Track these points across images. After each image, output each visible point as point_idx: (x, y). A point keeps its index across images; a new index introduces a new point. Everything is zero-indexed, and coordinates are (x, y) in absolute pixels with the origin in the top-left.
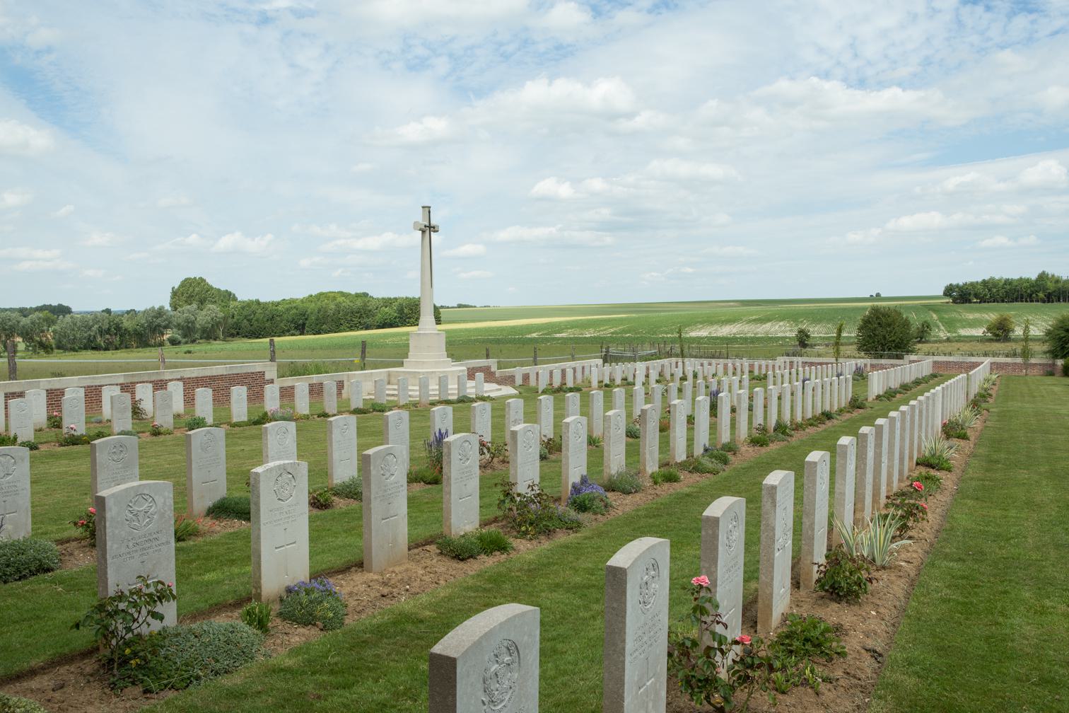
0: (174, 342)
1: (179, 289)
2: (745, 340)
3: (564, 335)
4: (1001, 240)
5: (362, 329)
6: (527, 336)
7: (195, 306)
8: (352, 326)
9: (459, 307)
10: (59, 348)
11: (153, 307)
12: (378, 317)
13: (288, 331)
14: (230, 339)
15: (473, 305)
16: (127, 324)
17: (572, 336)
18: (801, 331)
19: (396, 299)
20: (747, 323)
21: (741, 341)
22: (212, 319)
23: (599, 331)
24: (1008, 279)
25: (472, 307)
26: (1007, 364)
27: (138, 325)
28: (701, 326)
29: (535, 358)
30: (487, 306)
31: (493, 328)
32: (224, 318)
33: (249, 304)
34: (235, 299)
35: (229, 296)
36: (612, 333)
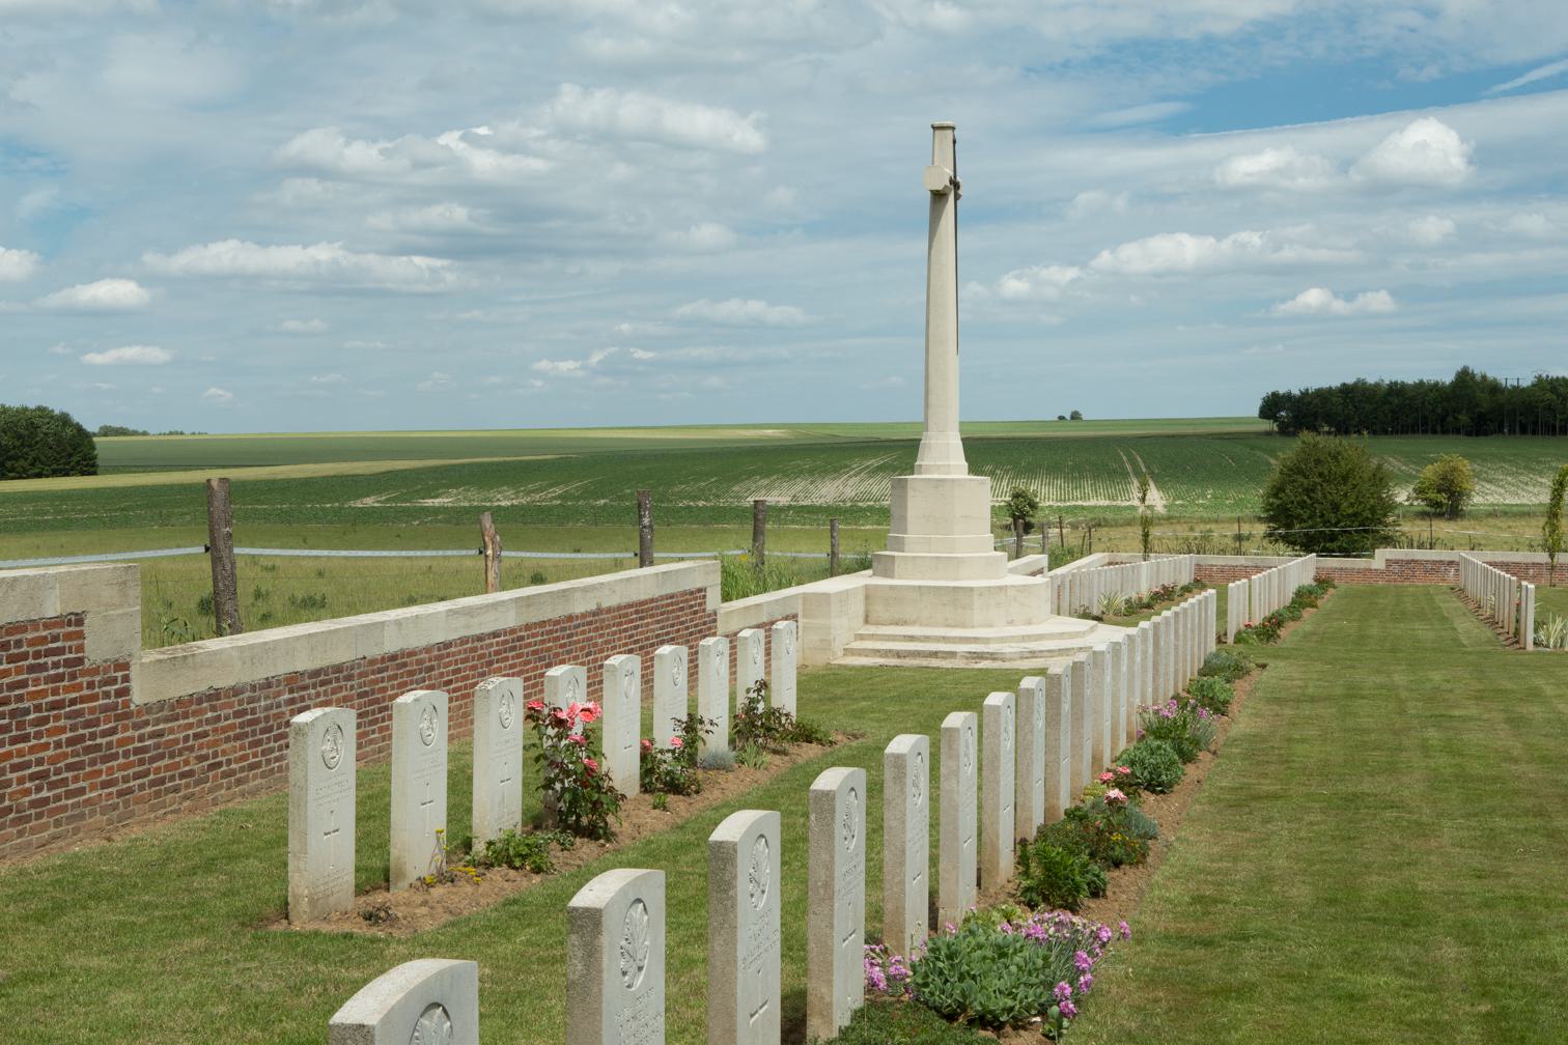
4: (1313, 297)
6: (352, 504)
9: (105, 435)
15: (141, 430)
24: (1396, 383)
25: (135, 433)
30: (177, 433)
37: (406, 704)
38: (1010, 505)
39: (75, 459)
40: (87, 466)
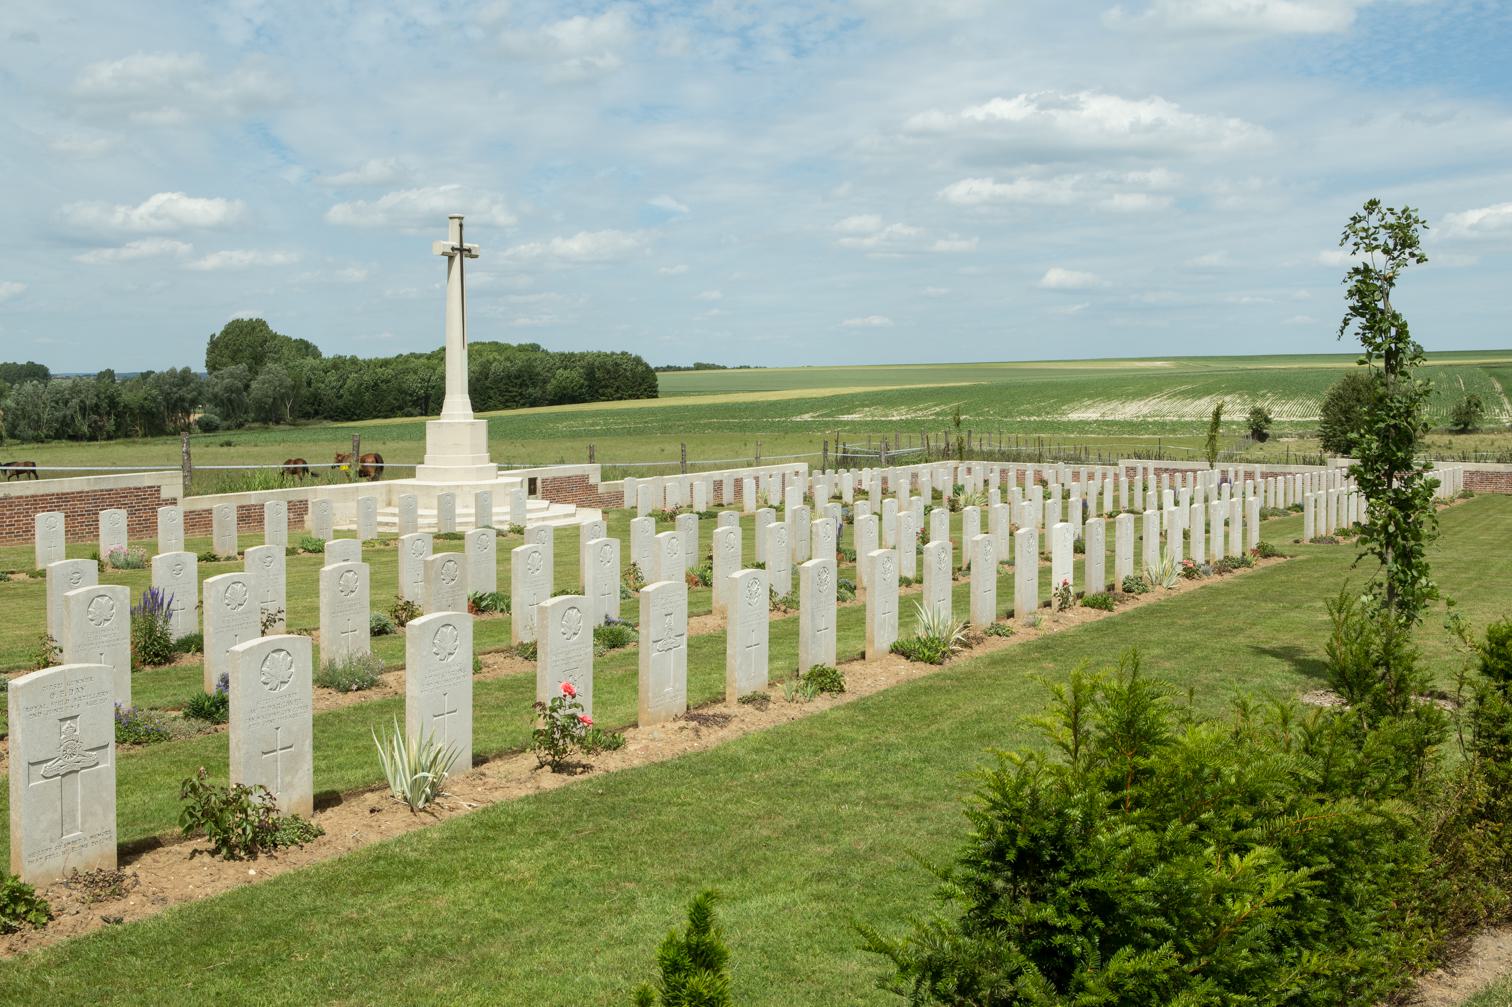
0: (207, 427)
2: (1162, 426)
3: (855, 417)
5: (523, 405)
6: (794, 419)
8: (507, 401)
10: (13, 436)
13: (400, 408)
14: (303, 421)
15: (721, 365)
16: (127, 397)
17: (869, 419)
18: (1257, 412)
19: (583, 356)
20: (1169, 398)
21: (1155, 429)
23: (915, 411)
25: (719, 368)
26: (1498, 475)
27: (146, 399)
28: (1089, 402)
29: (683, 462)
30: (745, 367)
31: (740, 404)
33: (338, 364)
34: (316, 354)
35: (305, 348)
36: (937, 414)
37: (648, 593)
38: (1249, 420)
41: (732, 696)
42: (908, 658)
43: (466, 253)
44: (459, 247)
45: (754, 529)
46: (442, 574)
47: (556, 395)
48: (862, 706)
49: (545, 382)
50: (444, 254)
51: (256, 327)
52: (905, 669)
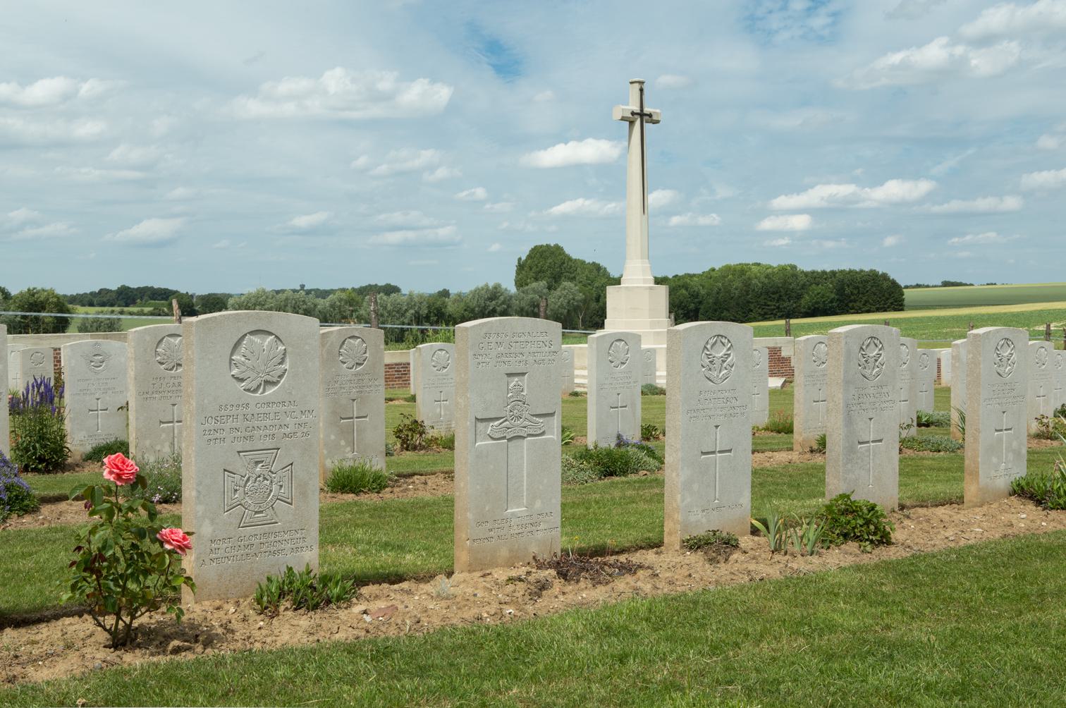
1: (526, 260)
6: (1037, 328)
7: (543, 284)
8: (766, 314)
11: (487, 285)
12: (806, 300)
19: (833, 273)
22: (569, 302)
25: (966, 285)
27: (465, 310)
30: (992, 284)
32: (585, 301)
39: (890, 301)
40: (897, 305)
41: (673, 539)
42: (1039, 503)
43: (647, 117)
44: (639, 111)
45: (935, 397)
46: (340, 354)
47: (809, 308)
48: (904, 572)
49: (799, 297)
50: (623, 119)
51: (556, 251)
52: (1026, 517)
